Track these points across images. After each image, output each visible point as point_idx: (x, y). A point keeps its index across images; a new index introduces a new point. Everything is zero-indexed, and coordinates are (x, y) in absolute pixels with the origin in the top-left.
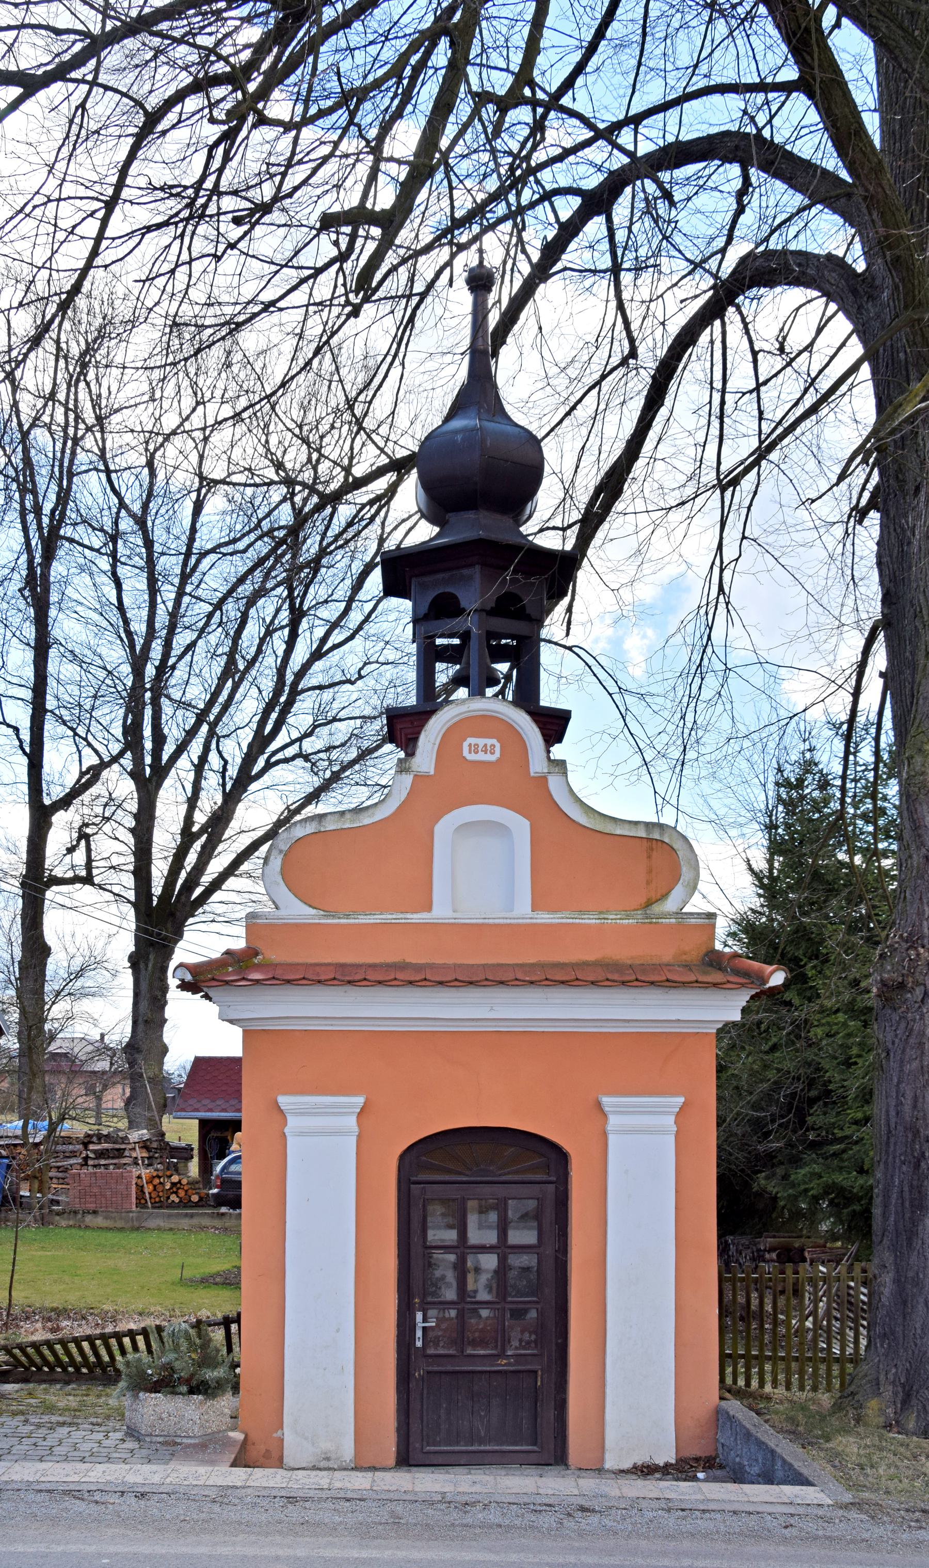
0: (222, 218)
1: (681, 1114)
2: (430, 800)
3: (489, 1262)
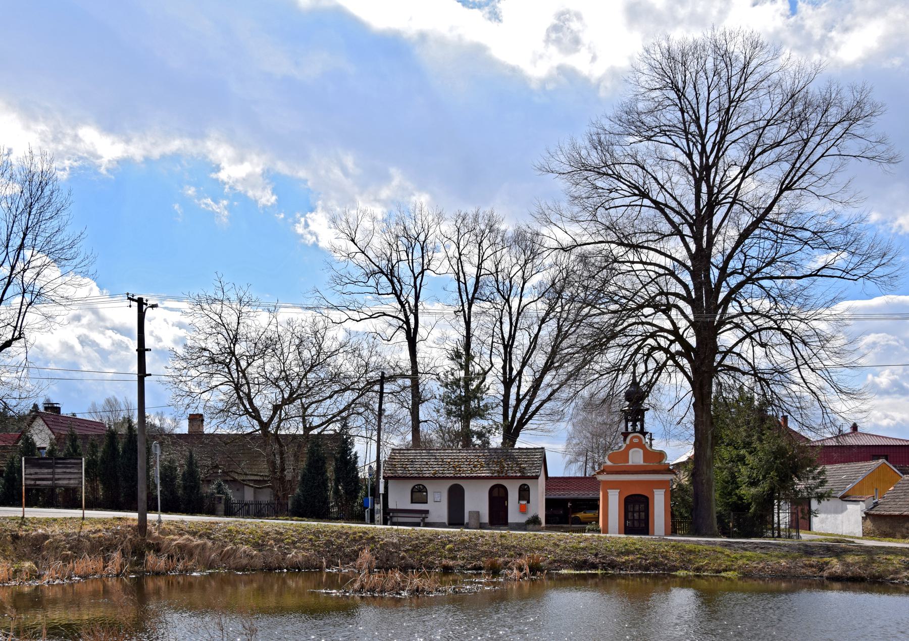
0: (388, 387)
2: (629, 447)
3: (664, 301)
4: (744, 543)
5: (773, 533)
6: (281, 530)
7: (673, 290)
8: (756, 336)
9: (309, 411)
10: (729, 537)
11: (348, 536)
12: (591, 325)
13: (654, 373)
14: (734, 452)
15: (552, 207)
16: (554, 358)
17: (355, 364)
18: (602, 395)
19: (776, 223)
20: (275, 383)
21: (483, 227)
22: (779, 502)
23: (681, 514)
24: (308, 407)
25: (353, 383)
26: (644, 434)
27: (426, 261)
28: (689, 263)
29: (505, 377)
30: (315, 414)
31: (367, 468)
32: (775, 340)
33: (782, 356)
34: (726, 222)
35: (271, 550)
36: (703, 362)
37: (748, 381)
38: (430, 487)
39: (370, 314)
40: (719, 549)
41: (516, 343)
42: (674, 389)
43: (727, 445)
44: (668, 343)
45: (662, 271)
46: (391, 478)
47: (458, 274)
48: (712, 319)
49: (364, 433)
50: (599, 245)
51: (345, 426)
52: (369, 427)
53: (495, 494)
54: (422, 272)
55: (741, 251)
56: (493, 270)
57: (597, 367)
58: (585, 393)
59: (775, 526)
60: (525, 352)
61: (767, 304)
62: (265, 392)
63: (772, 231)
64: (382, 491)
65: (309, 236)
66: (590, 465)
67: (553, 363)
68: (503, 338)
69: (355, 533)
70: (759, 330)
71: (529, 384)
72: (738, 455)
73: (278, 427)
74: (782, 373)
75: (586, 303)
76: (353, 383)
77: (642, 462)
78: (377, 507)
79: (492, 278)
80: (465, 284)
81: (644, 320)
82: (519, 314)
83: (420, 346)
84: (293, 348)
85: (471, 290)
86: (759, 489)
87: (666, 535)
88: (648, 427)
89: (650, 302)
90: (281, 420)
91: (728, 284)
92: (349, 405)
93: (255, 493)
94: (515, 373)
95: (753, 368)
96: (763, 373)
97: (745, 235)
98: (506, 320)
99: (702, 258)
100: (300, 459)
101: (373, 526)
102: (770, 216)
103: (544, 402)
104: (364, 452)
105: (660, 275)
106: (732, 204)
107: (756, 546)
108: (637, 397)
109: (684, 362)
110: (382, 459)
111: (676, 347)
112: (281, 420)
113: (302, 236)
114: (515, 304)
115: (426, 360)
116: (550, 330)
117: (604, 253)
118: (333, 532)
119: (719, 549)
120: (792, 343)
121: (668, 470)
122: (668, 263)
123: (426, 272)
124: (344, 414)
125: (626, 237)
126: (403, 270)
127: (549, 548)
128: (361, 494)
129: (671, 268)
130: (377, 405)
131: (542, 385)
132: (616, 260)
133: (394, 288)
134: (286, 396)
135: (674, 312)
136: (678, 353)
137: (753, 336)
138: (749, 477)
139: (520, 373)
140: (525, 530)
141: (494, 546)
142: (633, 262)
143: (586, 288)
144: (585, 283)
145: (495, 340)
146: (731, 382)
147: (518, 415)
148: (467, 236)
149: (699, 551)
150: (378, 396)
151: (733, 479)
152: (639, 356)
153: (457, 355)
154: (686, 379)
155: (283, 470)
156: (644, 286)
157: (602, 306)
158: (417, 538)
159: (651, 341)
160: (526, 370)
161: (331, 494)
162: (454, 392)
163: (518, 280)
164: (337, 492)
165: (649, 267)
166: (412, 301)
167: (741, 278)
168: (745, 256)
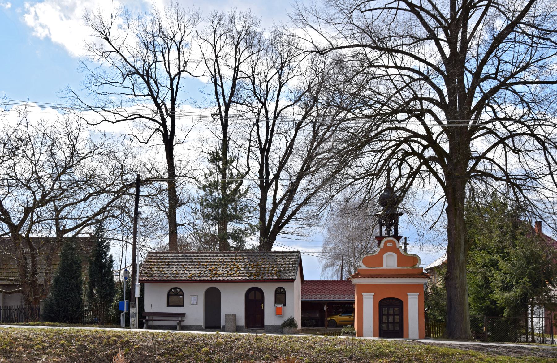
0: (144, 190)
1: (419, 296)
2: (384, 251)
3: (418, 106)
4: (497, 347)
5: (527, 338)
6: (31, 336)
7: (426, 96)
8: (509, 142)
9: (63, 214)
10: (483, 341)
11: (102, 341)
12: (346, 130)
13: (408, 178)
14: (488, 258)
15: (309, 8)
16: (311, 162)
17: (110, 166)
18: (357, 199)
19: (533, 26)
20: (27, 185)
21: (239, 28)
22: (533, 307)
23: (435, 317)
24: (62, 209)
25: (108, 186)
26: (398, 238)
27: (182, 63)
28: (443, 68)
29: (261, 181)
30: (69, 217)
31: (122, 272)
32: (528, 147)
33: (536, 162)
34: (480, 26)
35: (20, 357)
36: (456, 169)
37: (501, 186)
38: (187, 290)
39: (126, 116)
40: (472, 352)
41: (272, 148)
42: (427, 196)
43: (481, 250)
44: (422, 148)
45: (416, 76)
46: (147, 281)
47: (215, 77)
48: (465, 125)
49: (119, 236)
50: (355, 49)
51: (100, 229)
52: (125, 230)
53: (251, 297)
54: (179, 74)
55: (495, 56)
56: (250, 74)
57: (351, 172)
58: (340, 197)
59: (530, 330)
60: (282, 157)
61: (520, 111)
62: (15, 194)
63: (527, 35)
64: (137, 294)
65: (40, 29)
66: (346, 269)
67: (309, 167)
68: (260, 142)
69: (109, 337)
70: (512, 135)
71: (286, 189)
72: (491, 260)
73: (29, 231)
74: (535, 179)
75: (341, 108)
76: (108, 186)
77: (396, 266)
78: (132, 310)
79: (248, 81)
80: (222, 87)
81: (398, 125)
82: (275, 118)
83: (177, 150)
84: (44, 149)
85: (228, 92)
86: (512, 293)
87: (420, 338)
88: (402, 231)
89: (406, 108)
90: (32, 223)
91: (481, 89)
92: (104, 208)
93: (4, 298)
94: (271, 177)
95: (506, 173)
96: (515, 179)
97: (499, 39)
98: (263, 124)
99: (456, 62)
100: (53, 263)
101: (128, 330)
102: (525, 19)
103: (300, 206)
104: (120, 256)
105: (415, 80)
106: (487, 7)
107: (510, 351)
108: (391, 202)
109: (438, 168)
110: (138, 262)
111: (430, 153)
112: (32, 223)
113: (32, 29)
114: (271, 107)
115: (184, 163)
116: (306, 134)
117: (360, 56)
118: (86, 336)
119: (472, 352)
120: (545, 149)
121: (421, 274)
122: (423, 68)
123: (183, 74)
124: (99, 217)
125: (381, 40)
126: (160, 72)
127: (304, 350)
128: (116, 298)
129: (425, 73)
130: (133, 208)
131: (298, 189)
132: (371, 65)
133: (150, 90)
134: (38, 198)
135: (427, 118)
136: (432, 158)
137: (506, 141)
138: (502, 282)
139: (277, 177)
140: (281, 333)
141: (250, 349)
142: (388, 67)
143: (342, 93)
144: (341, 87)
145: (252, 144)
146: (483, 187)
147: (275, 219)
148: (223, 37)
149: (452, 355)
150: (134, 199)
151: (487, 284)
152: (393, 161)
153: (214, 158)
154: (439, 184)
155: (34, 273)
156: (398, 91)
157: (357, 111)
158: (173, 342)
159: (405, 146)
160: (283, 174)
161: (84, 297)
162: (211, 193)
163: (274, 83)
164: (91, 295)
165: (403, 72)
166: (169, 104)
167: (495, 83)
168: (499, 61)
